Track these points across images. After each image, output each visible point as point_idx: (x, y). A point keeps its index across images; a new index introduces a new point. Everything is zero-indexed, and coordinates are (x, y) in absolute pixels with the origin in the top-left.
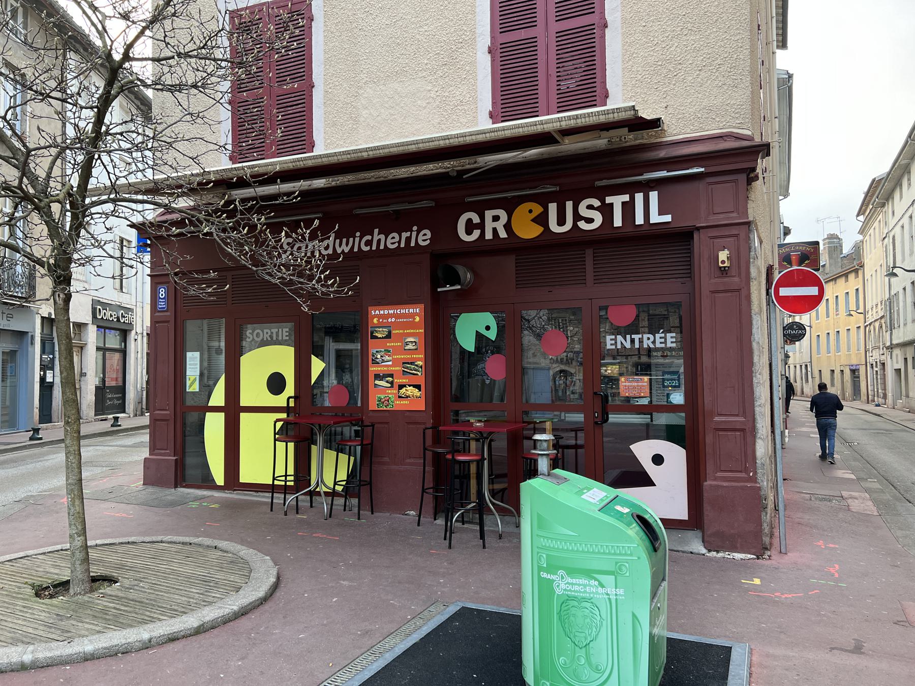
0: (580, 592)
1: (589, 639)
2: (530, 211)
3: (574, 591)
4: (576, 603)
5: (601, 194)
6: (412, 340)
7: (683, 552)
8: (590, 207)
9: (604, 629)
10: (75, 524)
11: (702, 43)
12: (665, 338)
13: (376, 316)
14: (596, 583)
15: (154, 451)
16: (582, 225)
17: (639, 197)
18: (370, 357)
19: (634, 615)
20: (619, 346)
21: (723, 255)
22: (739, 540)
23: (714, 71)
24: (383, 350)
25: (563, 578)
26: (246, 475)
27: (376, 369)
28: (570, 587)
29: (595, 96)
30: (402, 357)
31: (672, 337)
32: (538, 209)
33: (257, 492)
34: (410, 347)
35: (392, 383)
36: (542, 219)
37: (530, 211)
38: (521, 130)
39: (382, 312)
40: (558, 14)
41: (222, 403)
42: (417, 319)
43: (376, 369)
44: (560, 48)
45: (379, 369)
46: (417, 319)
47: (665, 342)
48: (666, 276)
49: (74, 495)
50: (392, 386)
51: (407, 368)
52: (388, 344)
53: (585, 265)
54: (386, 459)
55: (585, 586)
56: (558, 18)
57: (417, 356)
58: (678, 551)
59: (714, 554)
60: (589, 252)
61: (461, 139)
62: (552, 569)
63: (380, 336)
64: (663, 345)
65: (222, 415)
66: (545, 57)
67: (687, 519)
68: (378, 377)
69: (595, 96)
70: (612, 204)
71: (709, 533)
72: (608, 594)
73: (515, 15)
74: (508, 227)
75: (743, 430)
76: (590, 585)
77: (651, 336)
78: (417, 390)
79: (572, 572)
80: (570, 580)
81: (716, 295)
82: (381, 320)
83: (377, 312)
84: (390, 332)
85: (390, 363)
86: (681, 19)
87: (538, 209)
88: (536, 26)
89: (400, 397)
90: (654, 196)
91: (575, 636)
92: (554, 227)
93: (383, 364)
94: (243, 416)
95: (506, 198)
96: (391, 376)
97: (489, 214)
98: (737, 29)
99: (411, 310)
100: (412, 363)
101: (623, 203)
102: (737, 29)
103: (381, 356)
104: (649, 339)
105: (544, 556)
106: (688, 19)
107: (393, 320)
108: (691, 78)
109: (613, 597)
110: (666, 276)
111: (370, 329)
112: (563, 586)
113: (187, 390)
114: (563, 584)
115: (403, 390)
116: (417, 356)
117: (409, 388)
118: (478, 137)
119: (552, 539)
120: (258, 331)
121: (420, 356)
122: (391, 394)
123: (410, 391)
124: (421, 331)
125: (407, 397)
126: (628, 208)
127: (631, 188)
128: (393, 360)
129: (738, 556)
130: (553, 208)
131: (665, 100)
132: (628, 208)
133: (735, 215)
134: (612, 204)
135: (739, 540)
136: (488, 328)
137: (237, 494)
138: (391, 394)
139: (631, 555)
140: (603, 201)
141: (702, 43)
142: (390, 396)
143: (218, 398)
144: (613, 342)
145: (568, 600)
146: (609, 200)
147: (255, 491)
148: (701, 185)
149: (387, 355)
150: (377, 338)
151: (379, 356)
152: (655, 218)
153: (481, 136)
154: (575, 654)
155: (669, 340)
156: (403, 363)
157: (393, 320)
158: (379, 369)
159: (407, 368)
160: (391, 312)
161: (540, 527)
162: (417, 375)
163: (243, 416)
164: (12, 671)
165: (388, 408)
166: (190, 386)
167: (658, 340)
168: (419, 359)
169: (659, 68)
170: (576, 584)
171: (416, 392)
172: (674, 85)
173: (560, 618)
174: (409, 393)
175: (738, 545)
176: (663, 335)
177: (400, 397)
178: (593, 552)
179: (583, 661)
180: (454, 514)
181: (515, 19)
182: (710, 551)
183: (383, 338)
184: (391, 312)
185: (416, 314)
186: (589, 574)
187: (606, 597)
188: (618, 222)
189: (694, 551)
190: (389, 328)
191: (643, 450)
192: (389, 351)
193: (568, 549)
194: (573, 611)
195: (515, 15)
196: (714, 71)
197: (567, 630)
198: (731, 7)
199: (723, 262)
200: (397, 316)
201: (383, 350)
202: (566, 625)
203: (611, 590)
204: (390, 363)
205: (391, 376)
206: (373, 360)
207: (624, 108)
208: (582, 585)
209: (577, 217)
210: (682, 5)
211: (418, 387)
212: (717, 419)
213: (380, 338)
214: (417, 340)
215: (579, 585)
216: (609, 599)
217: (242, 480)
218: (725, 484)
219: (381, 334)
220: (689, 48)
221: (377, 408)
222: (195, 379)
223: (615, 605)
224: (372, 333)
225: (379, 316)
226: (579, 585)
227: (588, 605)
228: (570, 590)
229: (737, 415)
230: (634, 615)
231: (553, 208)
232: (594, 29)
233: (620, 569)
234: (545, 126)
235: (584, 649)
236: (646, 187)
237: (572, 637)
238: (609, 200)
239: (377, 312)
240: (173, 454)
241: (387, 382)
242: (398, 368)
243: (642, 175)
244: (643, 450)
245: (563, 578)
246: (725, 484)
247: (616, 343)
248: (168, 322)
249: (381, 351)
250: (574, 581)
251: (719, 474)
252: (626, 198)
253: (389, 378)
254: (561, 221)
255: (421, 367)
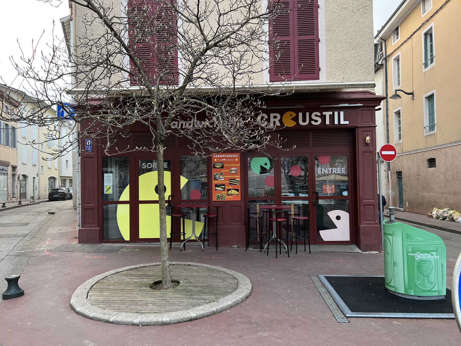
0: (425, 258)
1: (429, 273)
2: (291, 115)
3: (423, 258)
4: (424, 262)
5: (321, 110)
6: (234, 169)
7: (354, 253)
8: (316, 116)
9: (433, 269)
10: (166, 255)
11: (357, 54)
12: (341, 169)
13: (216, 158)
14: (431, 255)
15: (84, 225)
16: (313, 122)
17: (336, 113)
18: (213, 177)
19: (442, 264)
20: (323, 173)
21: (368, 138)
22: (373, 247)
23: (361, 66)
24: (219, 173)
25: (419, 254)
26: (143, 235)
27: (216, 182)
28: (422, 257)
29: (315, 69)
30: (229, 177)
31: (166, 164)
32: (294, 115)
33: (150, 242)
34: (233, 172)
35: (224, 188)
36: (296, 119)
37: (291, 115)
38: (329, 87)
39: (219, 156)
40: (299, 32)
41: (128, 199)
42: (237, 160)
43: (216, 182)
44: (300, 47)
45: (218, 182)
46: (237, 160)
47: (341, 171)
48: (342, 145)
49: (166, 242)
50: (224, 190)
51: (232, 182)
52: (222, 171)
53: (309, 139)
54: (221, 223)
55: (427, 256)
56: (299, 34)
57: (237, 176)
58: (352, 253)
59: (364, 253)
60: (311, 134)
61: (303, 88)
62: (414, 251)
63: (218, 167)
64: (340, 173)
65: (128, 206)
66: (293, 50)
67: (349, 240)
68: (217, 186)
69: (315, 69)
70: (325, 115)
71: (362, 245)
72: (434, 258)
73: (280, 29)
74: (281, 121)
75: (374, 205)
76: (428, 256)
77: (336, 169)
78: (237, 191)
79: (422, 252)
80: (421, 255)
81: (364, 153)
82: (218, 160)
83: (216, 156)
84: (223, 165)
85: (223, 179)
86: (349, 44)
87: (294, 115)
88: (289, 36)
89: (228, 195)
90: (342, 113)
91: (424, 273)
92: (301, 123)
93: (219, 180)
94: (141, 206)
95: (280, 109)
96: (224, 185)
97: (272, 115)
98: (370, 51)
99: (234, 156)
100: (234, 180)
101: (330, 115)
102: (370, 51)
103: (219, 176)
104: (335, 170)
105: (410, 248)
106: (352, 44)
107: (225, 160)
108: (353, 68)
109: (436, 259)
110: (342, 145)
111: (213, 164)
112: (419, 257)
113: (105, 193)
114: (419, 256)
115: (230, 192)
116: (237, 176)
117: (233, 191)
118: (311, 88)
119: (412, 242)
120: (149, 163)
121: (238, 176)
122: (223, 193)
123: (233, 192)
124: (238, 165)
125: (232, 195)
126: (332, 117)
127: (333, 109)
128: (225, 178)
129: (374, 252)
130: (300, 115)
131: (343, 75)
132: (332, 117)
133: (371, 123)
134: (325, 115)
135: (373, 247)
136: (266, 164)
137: (138, 244)
138: (223, 193)
139: (441, 244)
140: (322, 114)
141: (357, 54)
142: (223, 194)
143: (126, 195)
144: (340, 170)
145: (421, 262)
146: (324, 113)
147: (149, 242)
148: (359, 110)
149: (221, 176)
150: (216, 168)
151: (217, 176)
152: (342, 122)
153: (312, 88)
154: (424, 279)
155: (343, 170)
156: (230, 179)
157: (225, 160)
158: (218, 182)
159: (232, 182)
160: (224, 156)
161: (407, 238)
162: (237, 185)
163: (141, 206)
164: (211, 315)
165: (222, 200)
166: (107, 191)
167: (338, 170)
168: (238, 178)
169: (341, 62)
170: (424, 256)
171: (236, 192)
172: (346, 69)
173: (418, 268)
174: (233, 193)
175: (373, 249)
176: (340, 168)
177: (228, 195)
178: (429, 245)
179: (427, 281)
180: (263, 245)
181: (280, 31)
182: (363, 251)
183: (219, 168)
184: (224, 156)
185: (236, 157)
186: (428, 252)
187: (434, 259)
188: (328, 122)
189: (358, 252)
190: (223, 164)
191: (332, 214)
192: (223, 174)
193: (419, 244)
194: (423, 265)
195: (280, 29)
196: (361, 66)
197: (421, 272)
198: (368, 42)
199: (368, 141)
200: (226, 158)
201: (219, 173)
202: (421, 270)
203: (435, 257)
204: (223, 179)
205: (224, 185)
206: (214, 178)
207: (371, 84)
208: (426, 256)
209: (311, 119)
210: (350, 38)
211: (237, 190)
212: (364, 201)
213: (218, 168)
214: (237, 169)
215: (425, 256)
216: (435, 260)
217: (141, 237)
218: (368, 226)
219: (219, 166)
220: (352, 56)
221: (216, 200)
222: (110, 187)
223: (436, 261)
224: (214, 165)
225: (217, 158)
226: (425, 256)
227: (428, 262)
228: (422, 258)
229: (372, 199)
230: (442, 264)
231: (300, 115)
232: (314, 41)
233: (438, 250)
234: (339, 87)
235: (427, 277)
236: (340, 109)
237: (423, 274)
238: (324, 113)
239: (216, 156)
240: (97, 226)
241: (222, 188)
242: (227, 182)
243: (339, 104)
244: (332, 214)
245: (419, 254)
246: (368, 226)
247: (322, 171)
248: (93, 158)
249: (218, 174)
250: (423, 255)
251: (365, 222)
252: (331, 113)
253: (223, 186)
254: (304, 120)
255: (239, 181)
